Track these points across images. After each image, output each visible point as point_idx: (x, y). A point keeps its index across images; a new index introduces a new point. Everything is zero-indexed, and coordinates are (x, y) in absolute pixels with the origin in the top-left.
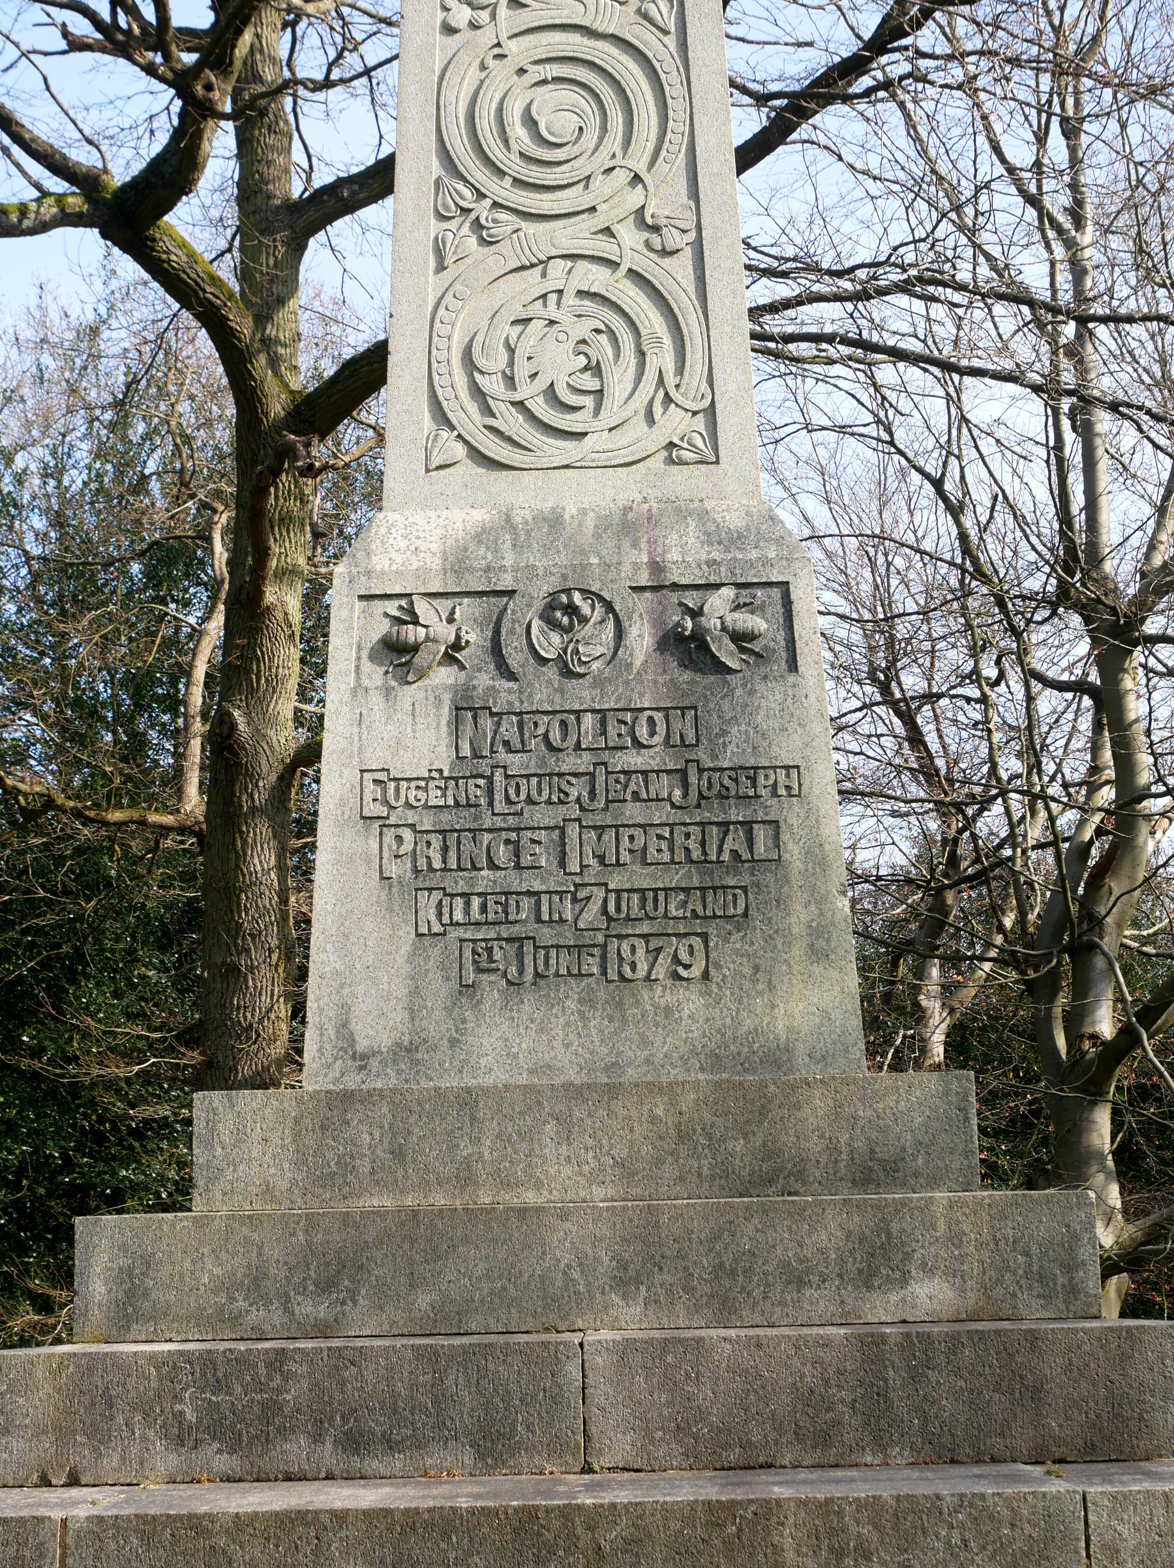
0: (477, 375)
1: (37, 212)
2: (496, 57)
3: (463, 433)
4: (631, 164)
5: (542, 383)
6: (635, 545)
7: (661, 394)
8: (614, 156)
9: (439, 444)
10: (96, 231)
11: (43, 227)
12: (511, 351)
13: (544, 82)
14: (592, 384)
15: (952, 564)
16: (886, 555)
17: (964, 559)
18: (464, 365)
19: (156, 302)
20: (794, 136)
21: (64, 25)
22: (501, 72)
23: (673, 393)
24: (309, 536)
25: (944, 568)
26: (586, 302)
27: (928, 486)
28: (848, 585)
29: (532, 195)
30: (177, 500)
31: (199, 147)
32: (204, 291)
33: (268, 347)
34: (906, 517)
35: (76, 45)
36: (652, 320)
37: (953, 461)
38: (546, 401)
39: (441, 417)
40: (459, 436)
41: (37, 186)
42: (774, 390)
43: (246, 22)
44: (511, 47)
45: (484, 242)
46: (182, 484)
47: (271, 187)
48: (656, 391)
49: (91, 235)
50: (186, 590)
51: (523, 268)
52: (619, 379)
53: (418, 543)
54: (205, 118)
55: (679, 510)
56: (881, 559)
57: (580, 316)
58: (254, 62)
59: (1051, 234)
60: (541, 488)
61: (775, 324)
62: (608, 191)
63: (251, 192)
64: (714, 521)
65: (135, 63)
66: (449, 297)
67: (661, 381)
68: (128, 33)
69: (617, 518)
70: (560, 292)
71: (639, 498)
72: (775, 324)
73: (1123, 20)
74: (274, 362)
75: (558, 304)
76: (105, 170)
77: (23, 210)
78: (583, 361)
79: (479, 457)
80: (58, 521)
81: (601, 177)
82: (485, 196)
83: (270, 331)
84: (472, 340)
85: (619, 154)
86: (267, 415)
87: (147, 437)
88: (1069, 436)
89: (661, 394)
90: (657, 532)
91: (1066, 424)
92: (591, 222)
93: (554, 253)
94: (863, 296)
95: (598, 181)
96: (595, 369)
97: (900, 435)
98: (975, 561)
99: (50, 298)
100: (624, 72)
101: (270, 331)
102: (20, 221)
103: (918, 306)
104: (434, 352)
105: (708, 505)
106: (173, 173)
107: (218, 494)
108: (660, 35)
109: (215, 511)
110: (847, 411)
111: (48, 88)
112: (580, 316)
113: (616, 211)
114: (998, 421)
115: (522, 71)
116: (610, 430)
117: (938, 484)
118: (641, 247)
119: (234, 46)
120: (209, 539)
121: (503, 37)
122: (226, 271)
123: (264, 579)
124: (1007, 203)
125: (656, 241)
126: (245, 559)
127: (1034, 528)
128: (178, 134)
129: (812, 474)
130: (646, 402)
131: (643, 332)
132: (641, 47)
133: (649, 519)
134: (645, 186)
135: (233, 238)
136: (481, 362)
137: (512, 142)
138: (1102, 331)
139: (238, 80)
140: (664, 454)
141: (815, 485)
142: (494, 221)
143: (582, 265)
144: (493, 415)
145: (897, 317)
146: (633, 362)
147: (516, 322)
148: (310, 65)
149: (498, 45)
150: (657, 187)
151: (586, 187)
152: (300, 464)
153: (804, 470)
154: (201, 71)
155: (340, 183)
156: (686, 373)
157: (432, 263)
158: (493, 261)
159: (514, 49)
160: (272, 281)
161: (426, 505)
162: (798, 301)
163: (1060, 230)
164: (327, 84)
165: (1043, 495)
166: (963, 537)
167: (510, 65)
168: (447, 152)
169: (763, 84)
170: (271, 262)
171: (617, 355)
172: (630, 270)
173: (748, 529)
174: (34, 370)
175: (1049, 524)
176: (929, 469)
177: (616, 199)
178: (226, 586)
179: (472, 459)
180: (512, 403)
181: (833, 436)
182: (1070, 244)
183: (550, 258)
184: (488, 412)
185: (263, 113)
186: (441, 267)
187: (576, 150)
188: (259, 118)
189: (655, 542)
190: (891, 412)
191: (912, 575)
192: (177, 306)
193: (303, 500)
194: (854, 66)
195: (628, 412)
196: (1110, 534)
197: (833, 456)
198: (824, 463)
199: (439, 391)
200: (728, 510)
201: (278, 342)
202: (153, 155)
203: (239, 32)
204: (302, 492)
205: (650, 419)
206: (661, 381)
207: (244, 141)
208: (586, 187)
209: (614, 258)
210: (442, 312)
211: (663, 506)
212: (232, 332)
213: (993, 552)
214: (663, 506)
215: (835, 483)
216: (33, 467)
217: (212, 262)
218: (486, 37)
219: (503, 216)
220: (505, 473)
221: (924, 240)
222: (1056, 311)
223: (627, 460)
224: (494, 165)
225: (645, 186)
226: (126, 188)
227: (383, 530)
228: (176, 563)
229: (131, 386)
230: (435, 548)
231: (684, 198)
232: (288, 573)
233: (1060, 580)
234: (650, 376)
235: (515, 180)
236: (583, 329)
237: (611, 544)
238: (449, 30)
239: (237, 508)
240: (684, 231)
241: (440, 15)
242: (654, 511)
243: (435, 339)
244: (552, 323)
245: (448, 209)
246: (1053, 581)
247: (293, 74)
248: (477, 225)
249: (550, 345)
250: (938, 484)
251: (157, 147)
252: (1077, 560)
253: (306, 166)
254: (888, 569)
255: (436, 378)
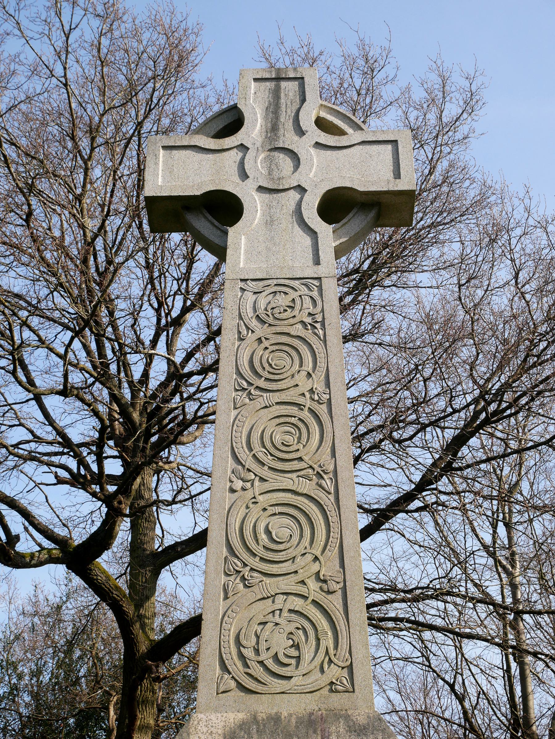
0: (241, 648)
1: (39, 557)
2: (253, 503)
3: (235, 676)
4: (314, 552)
5: (272, 652)
6: (315, 732)
7: (327, 659)
8: (306, 548)
9: (223, 681)
10: (64, 565)
11: (40, 564)
12: (258, 637)
13: (275, 514)
14: (295, 653)
15: (459, 725)
16: (428, 718)
17: (465, 723)
18: (236, 643)
19: (89, 598)
20: (383, 527)
21: (56, 472)
22: (256, 511)
23: (333, 658)
24: (155, 709)
25: (455, 727)
26: (293, 615)
27: (447, 687)
28: (410, 733)
29: (268, 565)
30: (93, 690)
31: (114, 529)
32: (113, 593)
33: (141, 619)
34: (437, 701)
35: (60, 481)
36: (323, 624)
37: (459, 676)
38: (274, 661)
39: (224, 668)
40: (233, 677)
41: (39, 545)
42: (374, 640)
43: (138, 475)
44: (260, 498)
45: (246, 586)
46: (96, 681)
47: (145, 546)
48: (325, 657)
49: (61, 569)
50: (95, 732)
51: (264, 598)
52: (308, 652)
53: (212, 729)
54: (117, 516)
55: (335, 715)
56: (425, 721)
57: (289, 621)
58: (140, 490)
59: (500, 569)
60: (271, 703)
61: (376, 612)
62: (303, 564)
63: (136, 548)
64: (352, 720)
65: (87, 492)
66: (229, 612)
67: (327, 653)
68: (85, 477)
69: (306, 718)
70: (281, 610)
71: (317, 709)
72: (376, 612)
73: (529, 476)
74: (143, 626)
75: (280, 615)
76: (71, 538)
77: (32, 555)
78: (291, 642)
79: (241, 687)
80: (35, 696)
81: (300, 557)
82: (247, 565)
83: (142, 611)
84: (239, 632)
85: (308, 547)
86: (138, 651)
87: (80, 658)
88: (514, 665)
89: (327, 659)
90: (325, 725)
91: (511, 657)
92: (295, 578)
93: (278, 591)
94: (416, 599)
95: (298, 559)
96: (296, 646)
97: (434, 663)
98: (471, 724)
99: (40, 591)
100: (311, 510)
101: (142, 611)
102: (30, 561)
103: (441, 605)
104: (222, 637)
105: (350, 712)
106: (102, 540)
107: (112, 687)
108: (327, 495)
109: (111, 695)
110: (408, 649)
111: (47, 501)
112: (289, 621)
113: (307, 573)
114: (480, 657)
115: (265, 509)
116: (303, 675)
117: (452, 687)
118: (318, 590)
119: (132, 485)
120: (107, 709)
121: (257, 493)
122: (122, 584)
123: (133, 730)
124: (482, 559)
125: (325, 587)
126: (125, 721)
127: (498, 706)
128: (104, 523)
129: (392, 679)
130: (320, 663)
131: (319, 629)
132: (319, 499)
133: (321, 719)
134: (320, 562)
135: (127, 569)
136: (244, 642)
137: (260, 541)
138: (526, 617)
139: (133, 499)
140: (329, 687)
141: (394, 684)
142: (251, 577)
143: (291, 598)
144: (249, 668)
145: (431, 611)
146: (314, 643)
147: (260, 624)
148: (166, 494)
149: (254, 498)
150: (325, 562)
151: (293, 562)
152: (153, 676)
153: (389, 677)
154: (117, 495)
155: (177, 544)
156: (339, 649)
157: (222, 595)
158: (251, 595)
159: (262, 500)
160: (143, 589)
161: (216, 710)
162: (385, 602)
163: (504, 567)
164: (174, 502)
165: (501, 690)
166: (465, 712)
167: (260, 506)
168: (230, 545)
169: (370, 504)
170: (144, 580)
171: (307, 640)
172: (313, 600)
173: (368, 725)
174: (30, 625)
175: (505, 709)
176: (447, 678)
177: (306, 567)
178: (115, 732)
179: (238, 688)
180: (258, 662)
181: (401, 663)
182: (510, 574)
183: (276, 594)
184: (246, 665)
185: (143, 513)
186: (226, 598)
187: (289, 545)
188: (143, 515)
189: (325, 730)
190: (429, 652)
191: (440, 728)
192: (99, 599)
193: (154, 692)
194: (409, 497)
195: (312, 667)
196: (535, 710)
197: (402, 671)
198: (398, 673)
199: (224, 656)
200: (359, 715)
201: (145, 617)
202: (93, 532)
203: (135, 479)
204: (153, 688)
205: (322, 671)
206: (327, 653)
207: (134, 527)
208: (293, 562)
209: (306, 595)
210: (226, 618)
211: (328, 713)
212: (124, 612)
213: (479, 720)
214: (328, 713)
215: (403, 684)
216: (26, 671)
217: (116, 579)
218: (249, 494)
219: (255, 574)
220: (254, 695)
221: (444, 577)
222: (506, 608)
223: (311, 690)
224: (251, 551)
225: (320, 562)
226: (79, 545)
227: (196, 723)
228: (91, 719)
229: (75, 634)
230: (220, 732)
231: (338, 567)
232: (144, 728)
233: (512, 734)
234: (322, 650)
235: (261, 558)
236: (291, 628)
237: (304, 731)
238: (232, 491)
239: (122, 694)
240: (338, 583)
241: (229, 484)
242: (324, 715)
243: (223, 631)
244: (277, 624)
245: (230, 571)
246: (508, 735)
247: (158, 496)
248: (243, 579)
249: (276, 635)
250: (452, 687)
251: (94, 529)
252: (519, 725)
253: (161, 536)
254: (429, 726)
255: (223, 649)
